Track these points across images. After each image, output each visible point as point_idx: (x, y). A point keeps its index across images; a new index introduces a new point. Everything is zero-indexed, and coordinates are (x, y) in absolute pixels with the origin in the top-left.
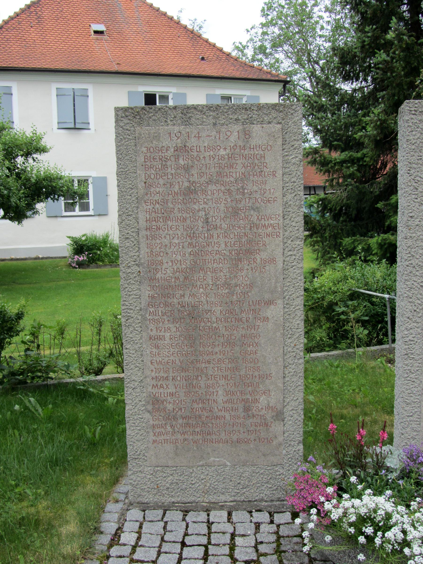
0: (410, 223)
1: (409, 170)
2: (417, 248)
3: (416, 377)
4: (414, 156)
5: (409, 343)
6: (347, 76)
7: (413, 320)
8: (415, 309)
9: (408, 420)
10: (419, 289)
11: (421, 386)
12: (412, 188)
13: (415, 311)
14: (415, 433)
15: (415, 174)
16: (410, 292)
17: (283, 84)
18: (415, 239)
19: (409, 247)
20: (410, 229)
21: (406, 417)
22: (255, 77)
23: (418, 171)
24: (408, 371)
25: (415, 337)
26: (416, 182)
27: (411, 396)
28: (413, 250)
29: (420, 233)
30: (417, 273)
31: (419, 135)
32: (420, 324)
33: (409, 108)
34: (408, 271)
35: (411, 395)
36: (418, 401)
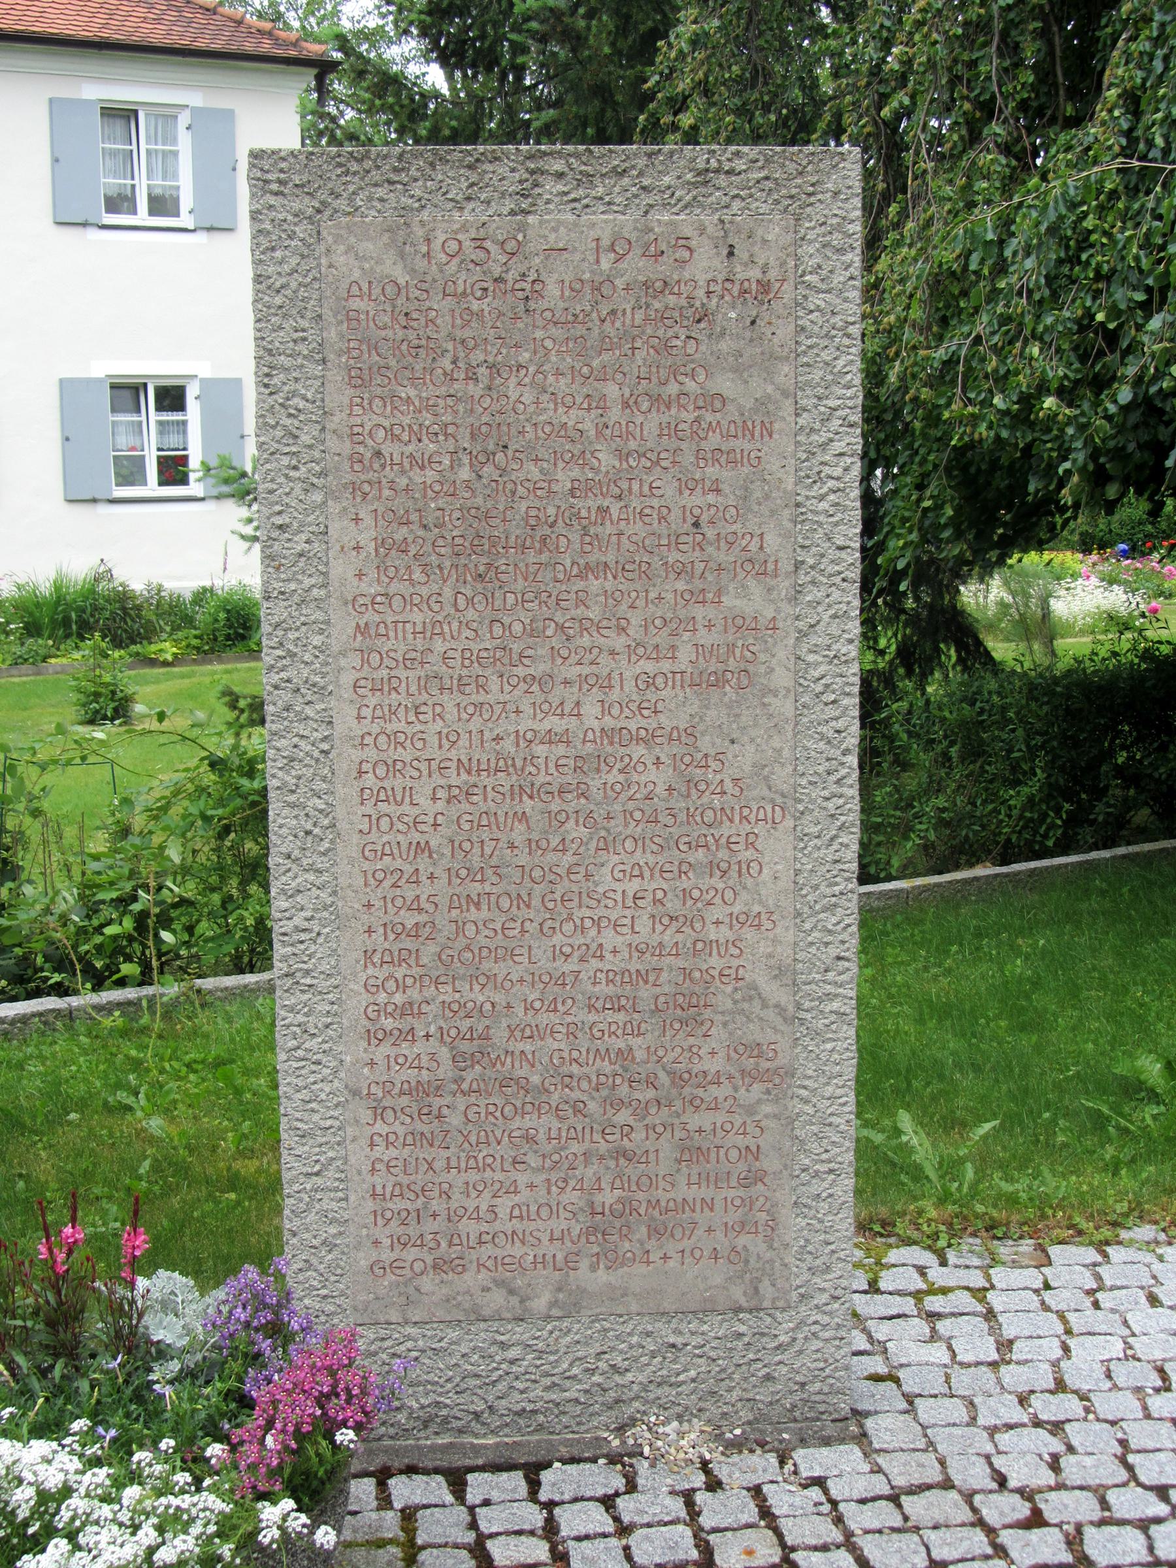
0: (277, 546)
1: (267, 375)
2: (304, 629)
3: (326, 1046)
4: (281, 328)
5: (295, 937)
6: (453, 54)
7: (305, 862)
8: (309, 827)
9: (308, 1186)
10: (317, 760)
11: (342, 1075)
12: (279, 433)
13: (308, 833)
14: (333, 1230)
15: (286, 388)
16: (288, 773)
17: (314, 71)
18: (296, 598)
19: (278, 625)
20: (278, 569)
21: (302, 1179)
22: (216, 46)
23: (297, 380)
24: (298, 1030)
25: (312, 918)
26: (290, 415)
27: (313, 1110)
28: (292, 635)
29: (313, 581)
30: (309, 711)
31: (294, 261)
32: (325, 877)
33: (259, 174)
34: (280, 703)
35: (314, 1105)
36: (337, 1123)
